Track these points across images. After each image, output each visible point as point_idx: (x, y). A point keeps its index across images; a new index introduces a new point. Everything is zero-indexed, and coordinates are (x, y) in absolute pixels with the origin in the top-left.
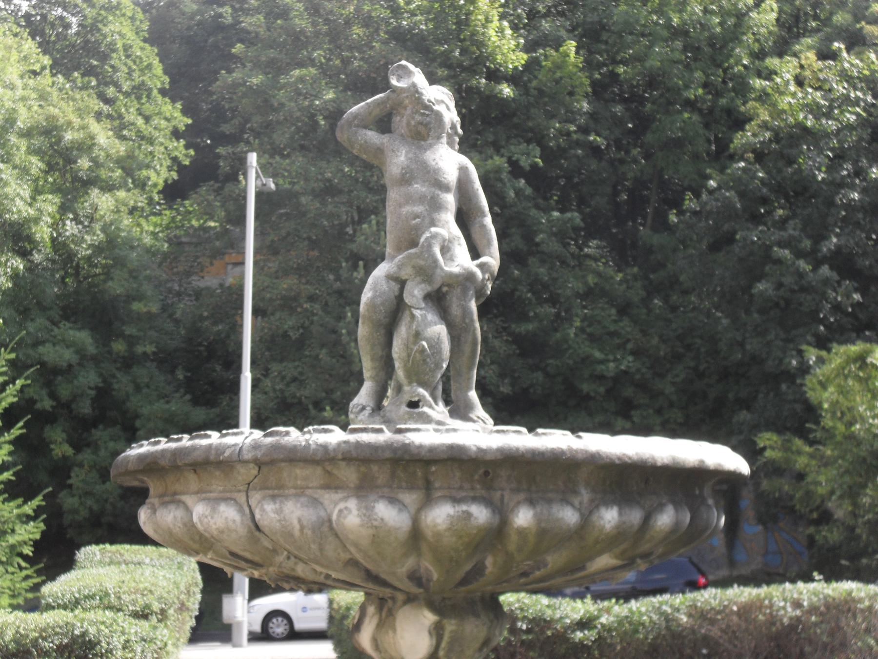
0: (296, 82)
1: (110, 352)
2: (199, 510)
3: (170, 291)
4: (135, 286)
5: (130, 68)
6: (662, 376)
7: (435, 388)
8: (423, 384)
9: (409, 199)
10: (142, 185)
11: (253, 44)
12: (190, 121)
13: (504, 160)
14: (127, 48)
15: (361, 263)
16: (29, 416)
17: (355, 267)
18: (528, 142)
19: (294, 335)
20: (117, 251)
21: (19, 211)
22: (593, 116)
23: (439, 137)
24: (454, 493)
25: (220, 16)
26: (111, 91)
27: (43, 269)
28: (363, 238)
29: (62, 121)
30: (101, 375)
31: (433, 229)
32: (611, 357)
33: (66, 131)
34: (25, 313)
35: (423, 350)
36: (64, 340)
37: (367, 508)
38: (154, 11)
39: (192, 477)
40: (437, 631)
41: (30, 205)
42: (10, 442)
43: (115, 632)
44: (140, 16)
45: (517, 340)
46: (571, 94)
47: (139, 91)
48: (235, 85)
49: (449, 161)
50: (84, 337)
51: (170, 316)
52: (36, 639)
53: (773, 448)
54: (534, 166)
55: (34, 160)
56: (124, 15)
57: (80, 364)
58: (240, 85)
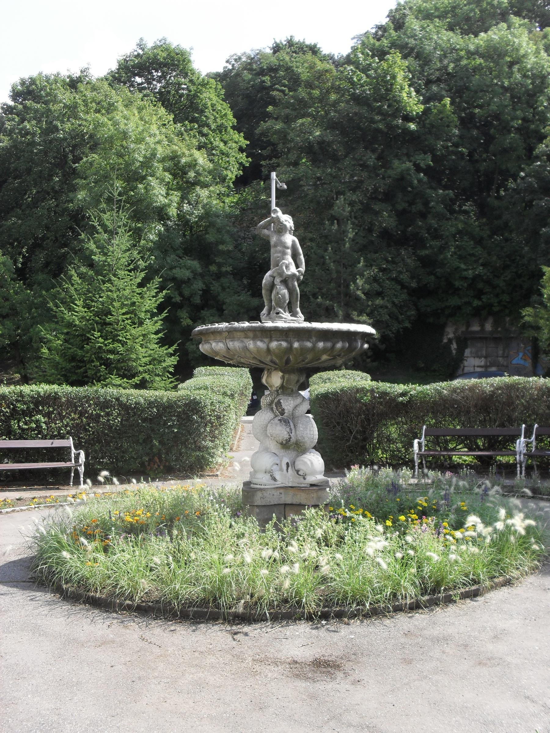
0: (300, 126)
1: (209, 271)
2: (214, 344)
3: (239, 237)
5: (215, 116)
8: (281, 308)
9: (276, 252)
10: (223, 180)
12: (248, 143)
13: (411, 164)
14: (213, 105)
17: (332, 224)
20: (210, 218)
22: (461, 137)
25: (264, 82)
26: (205, 130)
27: (173, 229)
30: (204, 283)
32: (470, 267)
33: (182, 157)
34: (165, 252)
36: (185, 266)
39: (212, 336)
40: (283, 378)
41: (166, 197)
42: (161, 320)
45: (421, 259)
46: (448, 126)
47: (221, 129)
49: (289, 239)
50: (195, 264)
51: (240, 250)
53: (529, 315)
54: (428, 166)
55: (167, 174)
56: (211, 87)
57: (194, 278)
58: (270, 129)
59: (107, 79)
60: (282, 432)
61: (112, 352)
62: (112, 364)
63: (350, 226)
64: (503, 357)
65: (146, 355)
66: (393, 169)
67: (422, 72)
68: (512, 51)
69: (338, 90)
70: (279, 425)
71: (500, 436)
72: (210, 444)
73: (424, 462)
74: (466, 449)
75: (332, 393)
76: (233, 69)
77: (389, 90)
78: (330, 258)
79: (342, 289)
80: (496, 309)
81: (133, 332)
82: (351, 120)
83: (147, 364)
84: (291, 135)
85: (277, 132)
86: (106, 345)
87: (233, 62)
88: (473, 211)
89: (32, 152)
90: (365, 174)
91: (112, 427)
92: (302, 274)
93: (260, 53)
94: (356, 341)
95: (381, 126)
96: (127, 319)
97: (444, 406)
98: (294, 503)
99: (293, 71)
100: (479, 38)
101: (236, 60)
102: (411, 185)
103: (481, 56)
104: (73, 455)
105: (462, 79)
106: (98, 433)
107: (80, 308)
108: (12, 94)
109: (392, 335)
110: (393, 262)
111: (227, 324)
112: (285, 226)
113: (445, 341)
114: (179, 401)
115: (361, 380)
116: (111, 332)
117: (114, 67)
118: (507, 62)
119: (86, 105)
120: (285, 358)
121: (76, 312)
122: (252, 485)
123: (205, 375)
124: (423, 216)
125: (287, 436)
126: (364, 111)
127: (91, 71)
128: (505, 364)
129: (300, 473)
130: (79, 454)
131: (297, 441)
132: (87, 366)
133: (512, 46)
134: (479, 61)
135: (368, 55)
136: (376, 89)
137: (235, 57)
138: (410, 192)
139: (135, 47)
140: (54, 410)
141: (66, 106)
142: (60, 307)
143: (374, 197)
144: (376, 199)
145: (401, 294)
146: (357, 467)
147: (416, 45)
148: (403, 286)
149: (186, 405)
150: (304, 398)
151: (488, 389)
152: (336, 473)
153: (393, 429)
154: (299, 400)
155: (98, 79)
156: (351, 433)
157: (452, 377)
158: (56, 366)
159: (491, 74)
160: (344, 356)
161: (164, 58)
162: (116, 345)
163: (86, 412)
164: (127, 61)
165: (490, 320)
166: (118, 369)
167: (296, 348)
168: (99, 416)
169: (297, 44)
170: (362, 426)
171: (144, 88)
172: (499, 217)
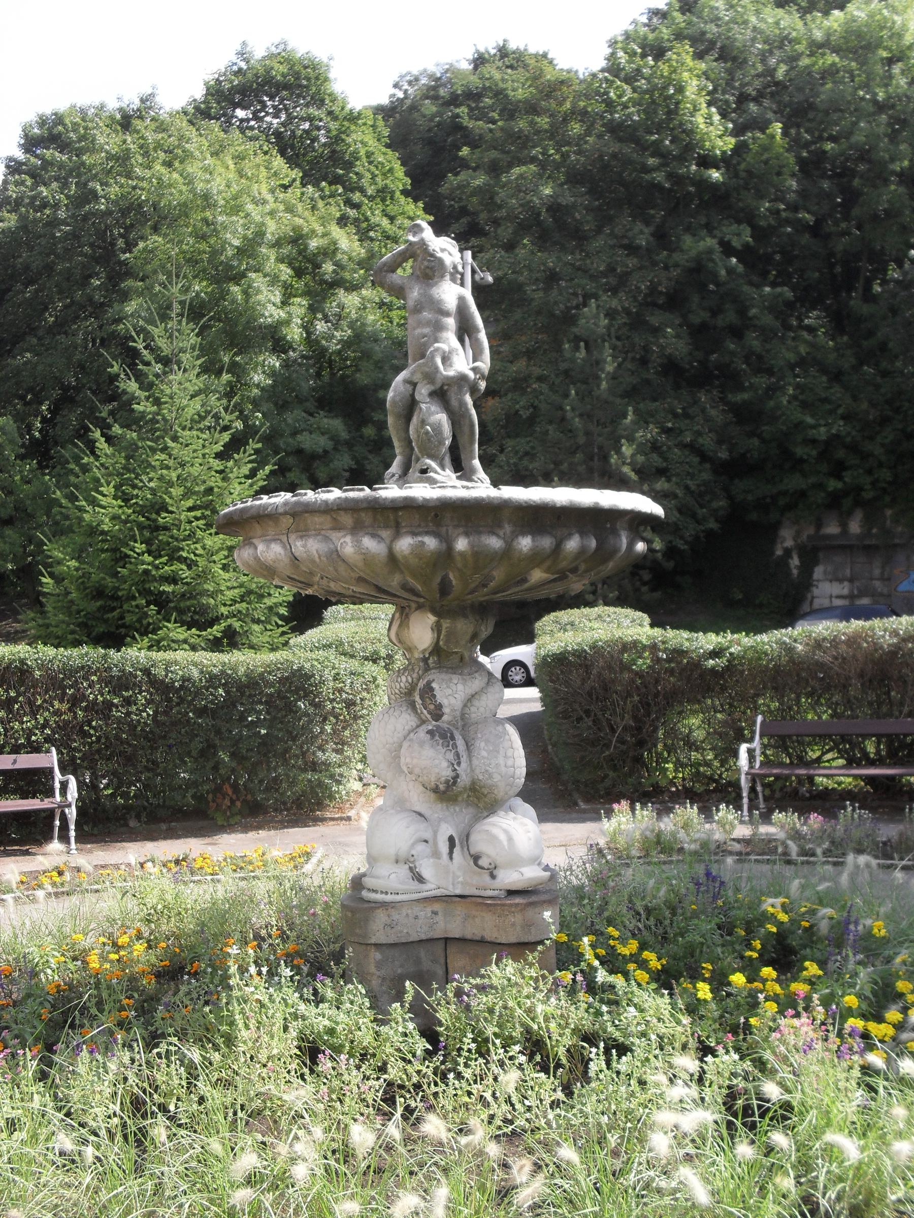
0: (517, 179)
1: (362, 437)
4: (381, 375)
5: (372, 173)
6: (871, 438)
7: (443, 459)
8: (432, 457)
9: (420, 324)
11: (477, 147)
14: (369, 155)
15: (582, 344)
16: (658, 510)
17: (577, 348)
18: (739, 222)
19: (525, 414)
20: (363, 344)
21: (271, 316)
22: (803, 193)
23: (442, 276)
24: (414, 529)
25: (458, 116)
26: (356, 197)
28: (584, 321)
29: (306, 230)
30: (354, 458)
31: (436, 345)
33: (311, 238)
34: (283, 406)
35: (427, 433)
36: (319, 428)
37: (357, 541)
38: (397, 115)
40: (437, 628)
43: (327, 667)
44: (380, 123)
47: (384, 194)
48: (460, 187)
50: (337, 424)
52: (263, 673)
55: (283, 267)
56: (365, 124)
57: (335, 449)
59: (185, 113)
60: (435, 762)
61: (173, 579)
62: (171, 601)
63: (608, 351)
64: (882, 579)
65: (235, 584)
66: (682, 251)
67: (729, 83)
68: (890, 37)
69: (583, 115)
70: (427, 746)
71: (908, 735)
72: (334, 758)
73: (759, 788)
74: (841, 762)
75: (575, 653)
76: (406, 98)
77: (672, 113)
78: (573, 409)
79: (596, 463)
80: (868, 495)
81: (209, 542)
82: (605, 167)
83: (235, 602)
84: (502, 194)
85: (479, 191)
86: (157, 568)
87: (406, 87)
88: (822, 326)
89: (54, 237)
90: (632, 262)
91: (136, 727)
92: (483, 377)
93: (451, 69)
94: (615, 533)
95: (659, 177)
96: (197, 519)
97: (798, 675)
98: (469, 936)
99: (506, 96)
100: (831, 18)
101: (410, 83)
102: (715, 276)
103: (836, 50)
104: (57, 785)
105: (800, 89)
106: (107, 738)
107: (110, 500)
108: (22, 141)
109: (683, 547)
110: (686, 415)
111: (289, 495)
112: (441, 262)
113: (779, 552)
114: (270, 673)
115: (627, 626)
116: (169, 544)
117: (199, 93)
118: (882, 59)
119: (146, 154)
120: (438, 580)
121: (104, 508)
122: (365, 894)
123: (345, 620)
124: (737, 333)
125: (447, 773)
126: (628, 149)
127: (158, 99)
128: (885, 591)
129: (480, 862)
130: (67, 782)
131: (473, 783)
132: (125, 607)
133: (891, 29)
134: (832, 58)
135: (635, 54)
136: (650, 109)
137: (408, 78)
138: (712, 292)
139: (234, 59)
140: (19, 695)
141: (110, 157)
142: (77, 499)
143: (650, 301)
144: (655, 305)
145: (700, 471)
146: (625, 804)
147: (720, 34)
148: (704, 457)
149: (282, 681)
150: (490, 674)
151: (889, 640)
152: (584, 811)
153: (694, 721)
154: (477, 683)
155: (171, 115)
156: (613, 731)
157: (788, 618)
158: (69, 608)
159: (853, 81)
160: (587, 571)
161: (283, 75)
162: (177, 566)
163: (84, 697)
164: (221, 82)
165: (859, 515)
166: (181, 612)
167: (462, 554)
168: (109, 705)
169: (514, 53)
170: (635, 718)
171: (252, 128)
172: (871, 334)
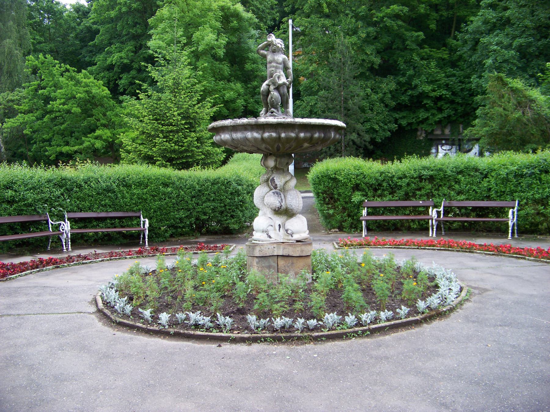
40: (276, 161)
50: (239, 86)
125: (279, 205)
154: (288, 178)
